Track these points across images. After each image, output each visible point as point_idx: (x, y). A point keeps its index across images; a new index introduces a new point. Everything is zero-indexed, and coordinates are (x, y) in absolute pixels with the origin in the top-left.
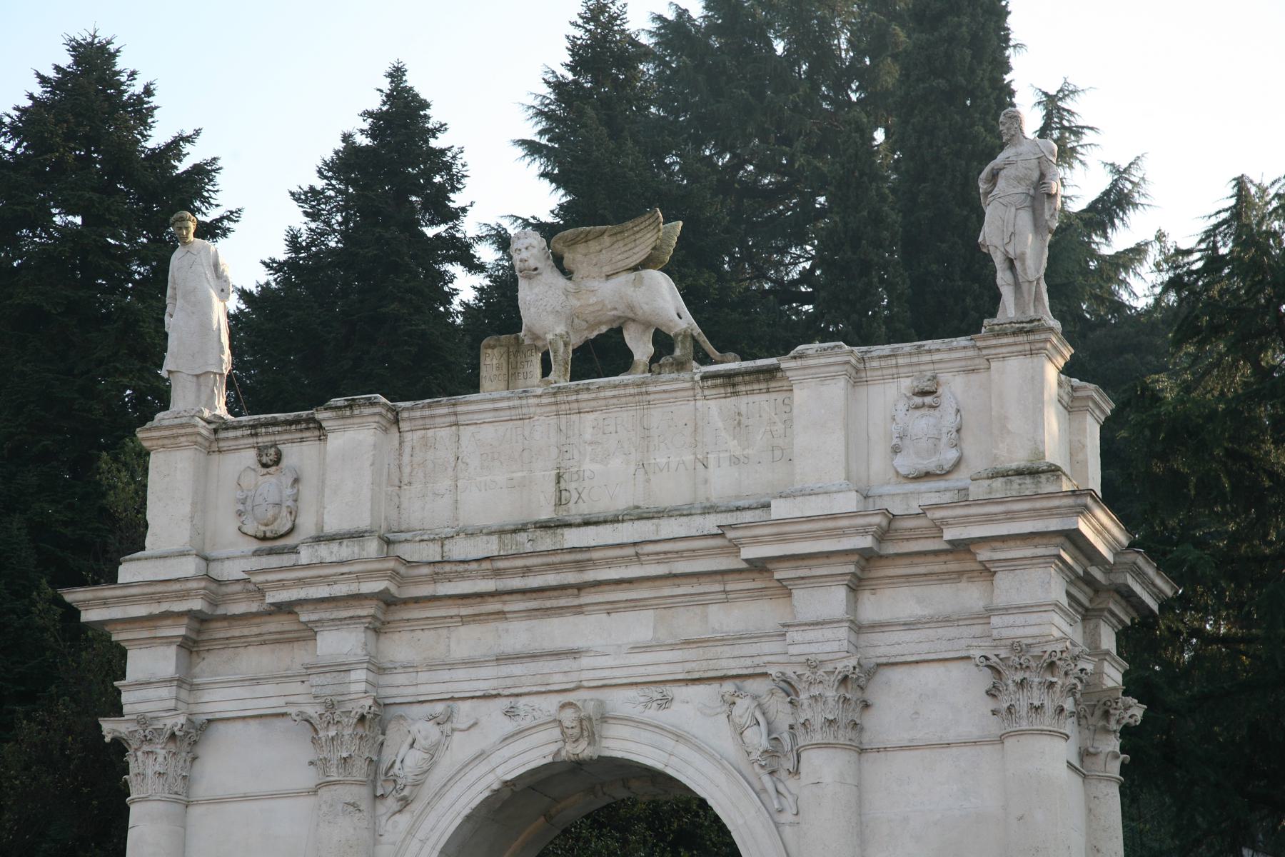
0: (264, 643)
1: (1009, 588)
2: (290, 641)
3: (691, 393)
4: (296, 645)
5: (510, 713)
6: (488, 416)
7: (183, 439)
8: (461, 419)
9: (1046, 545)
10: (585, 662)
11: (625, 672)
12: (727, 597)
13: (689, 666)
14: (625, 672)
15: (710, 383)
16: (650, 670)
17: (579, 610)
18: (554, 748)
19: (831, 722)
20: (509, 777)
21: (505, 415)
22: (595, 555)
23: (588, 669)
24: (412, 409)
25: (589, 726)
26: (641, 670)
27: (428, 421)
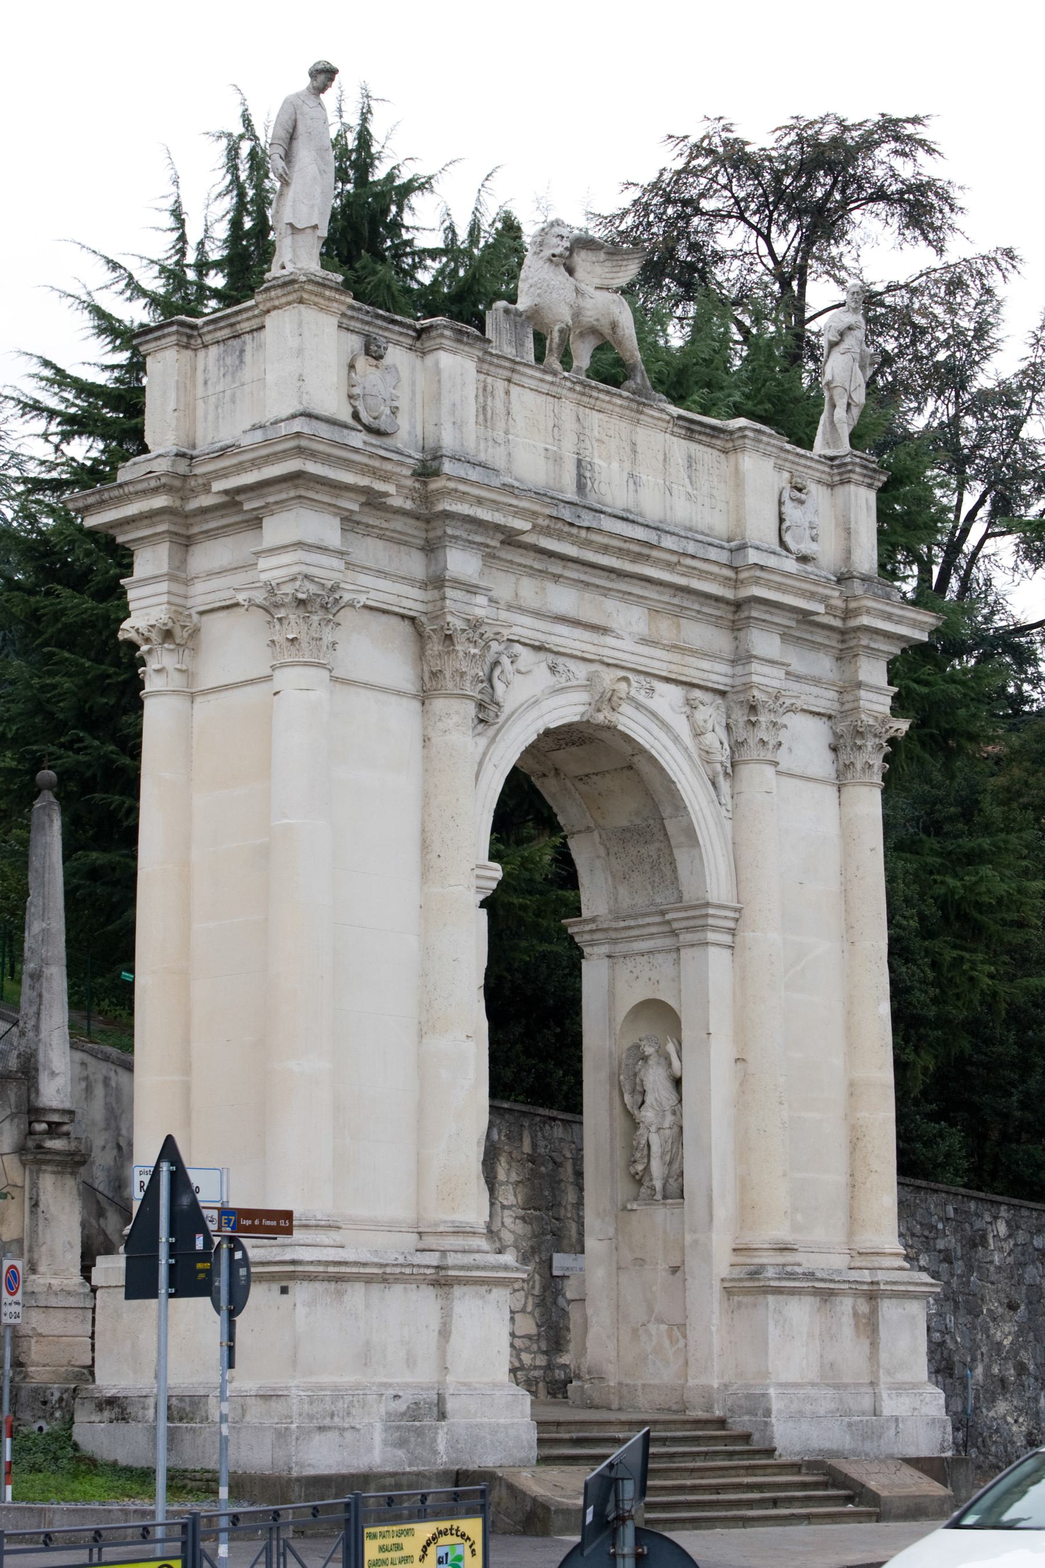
0: (390, 540)
1: (279, 528)
2: (400, 543)
3: (665, 425)
4: (402, 548)
5: (553, 669)
6: (533, 384)
7: (335, 305)
8: (516, 377)
9: (578, 571)
10: (609, 640)
11: (634, 658)
12: (700, 617)
13: (673, 667)
14: (634, 658)
15: (681, 423)
16: (642, 660)
17: (606, 592)
18: (582, 709)
19: (293, 640)
20: (552, 726)
21: (545, 388)
22: (655, 553)
23: (609, 647)
24: (770, 435)
25: (611, 701)
26: (642, 660)
27: (492, 368)
